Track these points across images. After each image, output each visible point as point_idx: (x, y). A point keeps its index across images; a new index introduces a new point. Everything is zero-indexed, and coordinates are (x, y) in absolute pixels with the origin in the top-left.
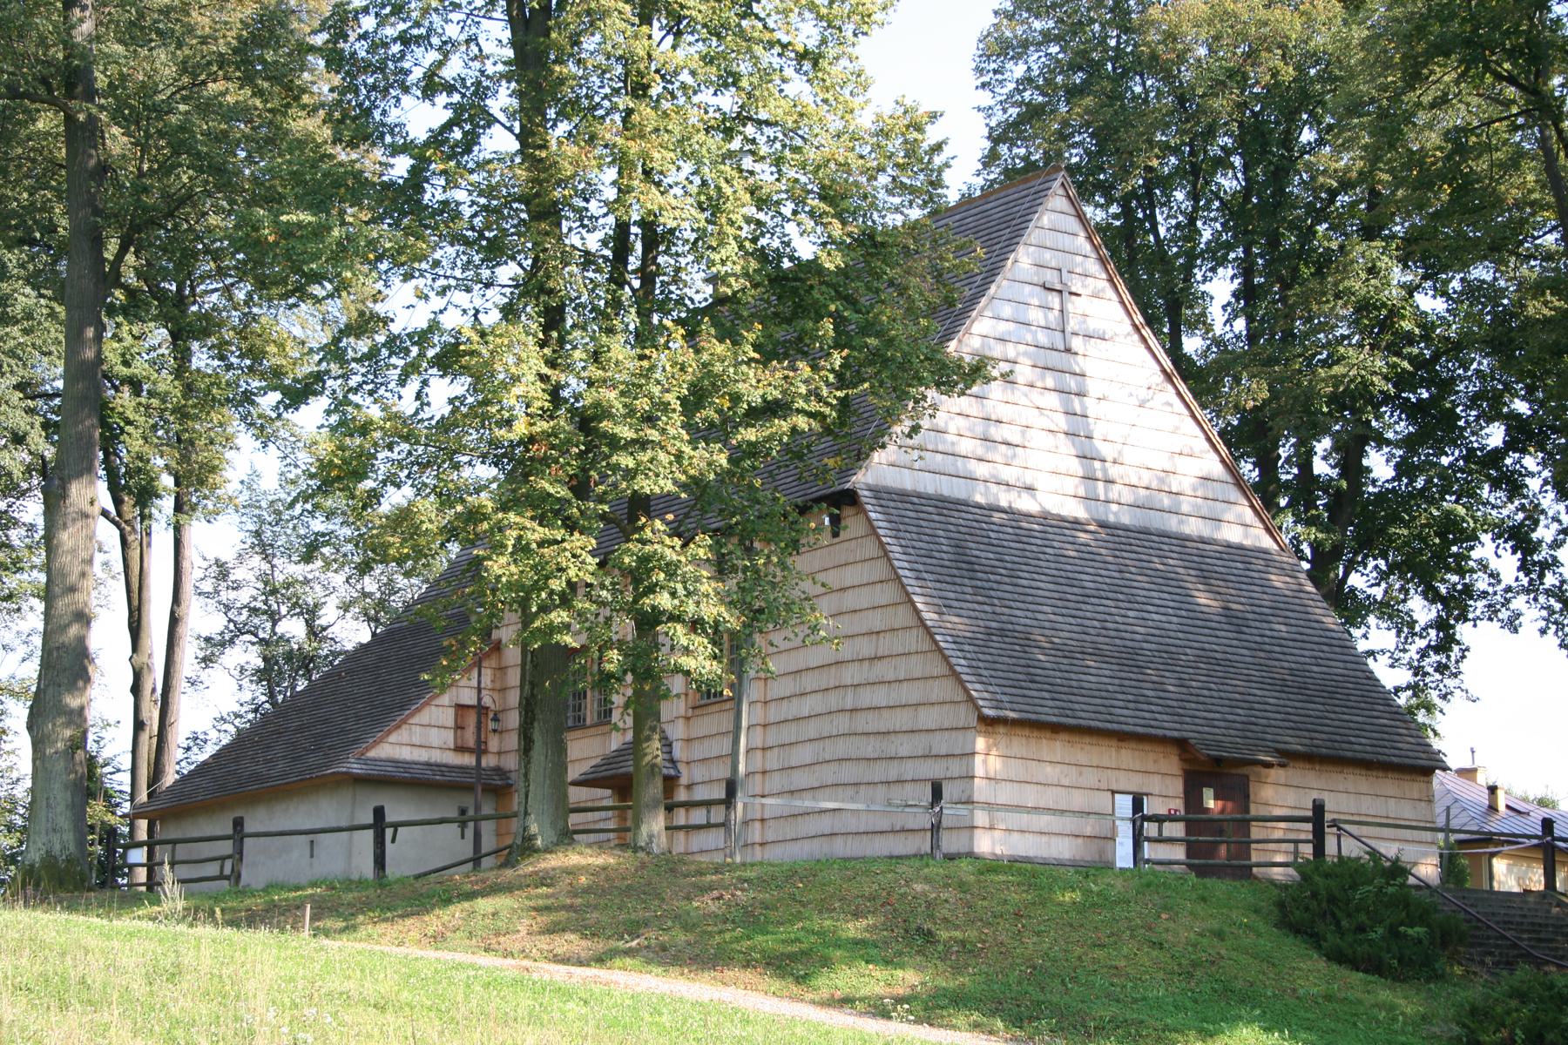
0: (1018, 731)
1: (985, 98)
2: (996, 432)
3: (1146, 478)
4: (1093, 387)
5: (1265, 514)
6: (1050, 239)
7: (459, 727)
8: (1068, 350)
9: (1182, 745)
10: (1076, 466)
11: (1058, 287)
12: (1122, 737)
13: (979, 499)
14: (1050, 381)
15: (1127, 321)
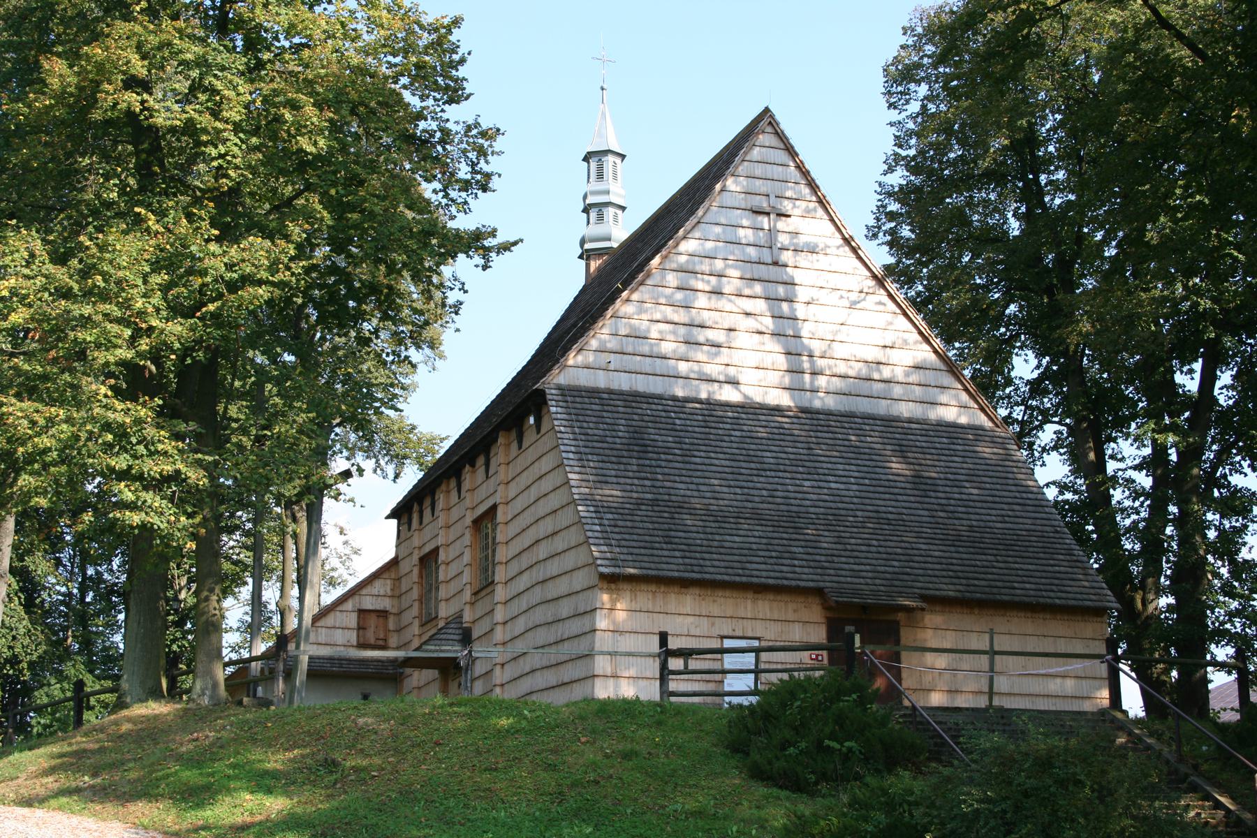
0: (644, 587)
1: (894, 115)
2: (701, 335)
3: (854, 369)
4: (802, 294)
5: (983, 401)
6: (759, 170)
7: (361, 628)
8: (776, 263)
9: (819, 592)
10: (782, 361)
11: (768, 209)
12: (760, 589)
13: (680, 393)
14: (758, 288)
15: (838, 235)
